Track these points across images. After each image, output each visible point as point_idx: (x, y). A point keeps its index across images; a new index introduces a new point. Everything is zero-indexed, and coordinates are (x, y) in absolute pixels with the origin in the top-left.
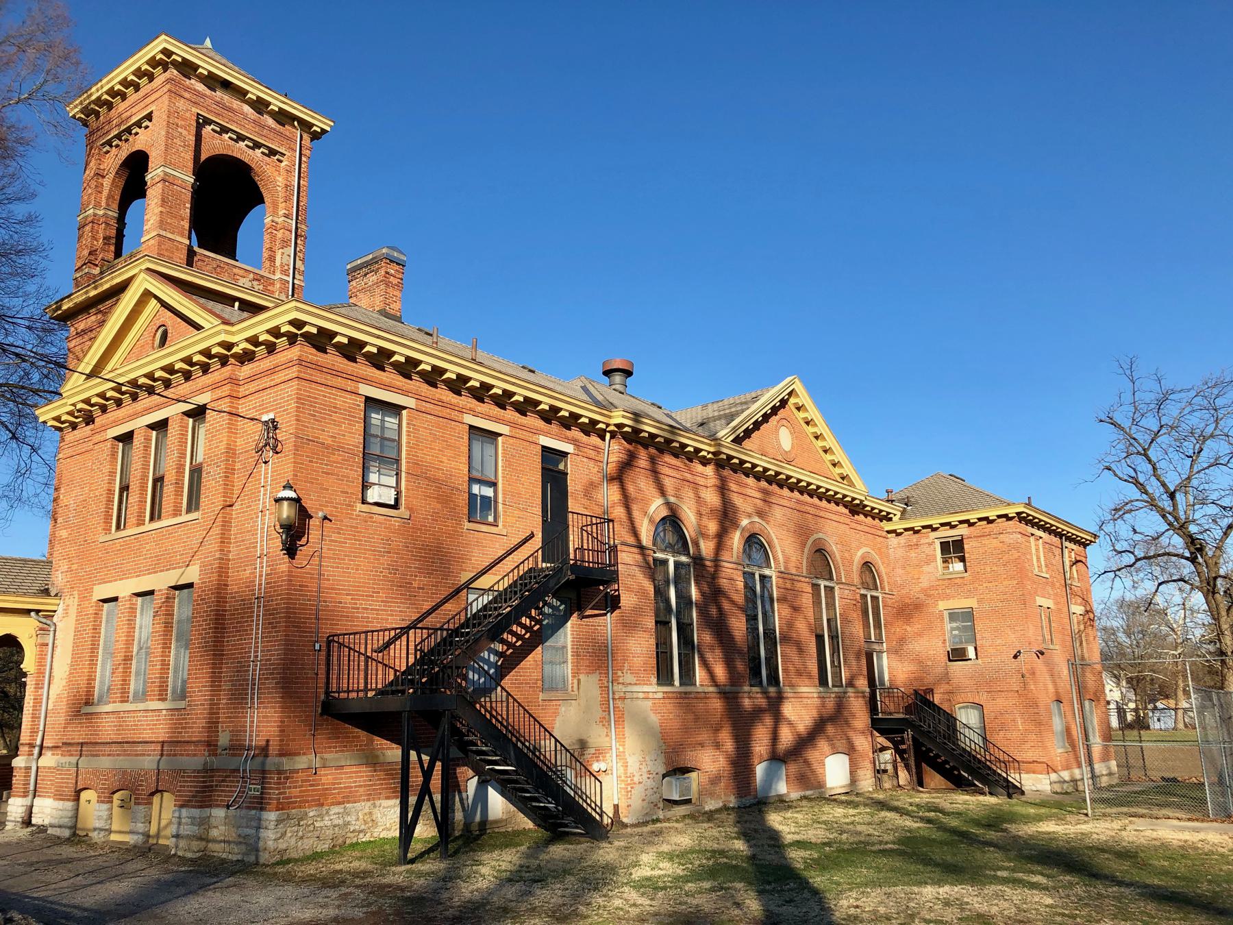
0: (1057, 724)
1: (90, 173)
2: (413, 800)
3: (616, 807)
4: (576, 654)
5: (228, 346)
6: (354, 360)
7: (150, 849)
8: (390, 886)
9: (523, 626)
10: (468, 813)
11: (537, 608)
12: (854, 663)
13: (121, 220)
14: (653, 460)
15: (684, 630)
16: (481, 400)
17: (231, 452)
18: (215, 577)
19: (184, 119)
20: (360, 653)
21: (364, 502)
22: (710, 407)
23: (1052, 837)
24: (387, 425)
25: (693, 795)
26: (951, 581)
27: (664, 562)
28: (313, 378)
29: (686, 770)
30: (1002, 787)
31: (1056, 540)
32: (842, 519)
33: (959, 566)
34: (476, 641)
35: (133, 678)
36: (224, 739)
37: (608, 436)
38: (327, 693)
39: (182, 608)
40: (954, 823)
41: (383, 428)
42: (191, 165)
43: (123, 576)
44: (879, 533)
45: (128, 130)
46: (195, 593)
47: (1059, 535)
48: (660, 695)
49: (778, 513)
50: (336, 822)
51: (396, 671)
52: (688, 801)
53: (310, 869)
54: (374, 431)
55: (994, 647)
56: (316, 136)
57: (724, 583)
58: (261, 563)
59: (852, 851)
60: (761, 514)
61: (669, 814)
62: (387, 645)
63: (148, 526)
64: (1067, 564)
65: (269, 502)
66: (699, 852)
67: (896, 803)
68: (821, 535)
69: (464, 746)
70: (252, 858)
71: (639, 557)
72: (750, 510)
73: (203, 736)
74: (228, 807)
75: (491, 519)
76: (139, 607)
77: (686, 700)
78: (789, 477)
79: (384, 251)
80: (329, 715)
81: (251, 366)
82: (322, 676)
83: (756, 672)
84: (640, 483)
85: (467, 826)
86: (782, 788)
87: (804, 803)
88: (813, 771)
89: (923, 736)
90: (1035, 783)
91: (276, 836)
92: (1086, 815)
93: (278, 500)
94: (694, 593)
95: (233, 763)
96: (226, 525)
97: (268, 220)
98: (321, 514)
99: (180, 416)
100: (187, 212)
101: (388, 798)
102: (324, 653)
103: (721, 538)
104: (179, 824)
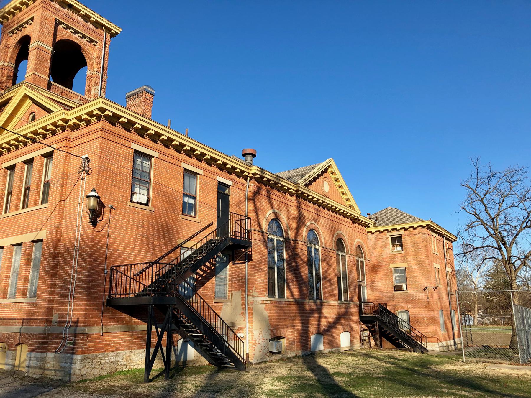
0: (441, 320)
1: (2, 45)
2: (152, 350)
3: (247, 355)
4: (231, 281)
5: (66, 121)
6: (129, 131)
7: (15, 373)
8: (140, 394)
9: (207, 267)
10: (178, 356)
11: (213, 258)
12: (353, 290)
13: (16, 68)
14: (268, 192)
15: (281, 272)
16: (190, 157)
17: (65, 174)
18: (54, 236)
19: (48, 20)
20: (127, 276)
21: (131, 201)
22: (292, 171)
23: (470, 371)
24: (144, 165)
25: (282, 350)
26: (396, 255)
27: (272, 240)
28: (109, 138)
29: (280, 338)
30: (419, 348)
31: (441, 238)
32: (349, 225)
33: (399, 248)
34: (185, 272)
35: (9, 287)
36: (55, 318)
37: (249, 179)
38: (110, 295)
39: (36, 252)
40: (405, 365)
41: (142, 166)
42: (51, 42)
43: (7, 235)
44: (364, 232)
45: (22, 26)
46: (43, 244)
47: (443, 236)
48: (269, 302)
49: (322, 220)
50: (112, 360)
51: (144, 286)
52: (280, 353)
53: (98, 385)
54: (138, 167)
55: (415, 285)
56: (113, 35)
57: (298, 250)
58: (78, 229)
59: (364, 378)
60: (315, 220)
61: (272, 359)
62: (141, 272)
63: (21, 211)
64: (445, 249)
65: (84, 198)
66: (292, 377)
67: (374, 355)
68: (340, 232)
69: (178, 323)
70: (67, 379)
71: (261, 237)
72: (310, 218)
73: (44, 316)
74: (56, 352)
75: (193, 214)
76: (14, 251)
77: (280, 305)
78: (328, 204)
79: (145, 87)
80: (110, 306)
81: (77, 132)
82: (108, 286)
83: (311, 294)
84: (263, 202)
85: (177, 363)
86: (322, 347)
87: (332, 354)
88: (335, 340)
89: (382, 324)
90: (433, 347)
91: (80, 367)
92: (463, 361)
93: (88, 197)
94: (285, 255)
95: (59, 330)
96: (61, 210)
97: (88, 73)
98: (110, 206)
99: (40, 157)
100: (48, 64)
101: (138, 349)
102: (109, 275)
103: (298, 230)
104: (30, 360)
